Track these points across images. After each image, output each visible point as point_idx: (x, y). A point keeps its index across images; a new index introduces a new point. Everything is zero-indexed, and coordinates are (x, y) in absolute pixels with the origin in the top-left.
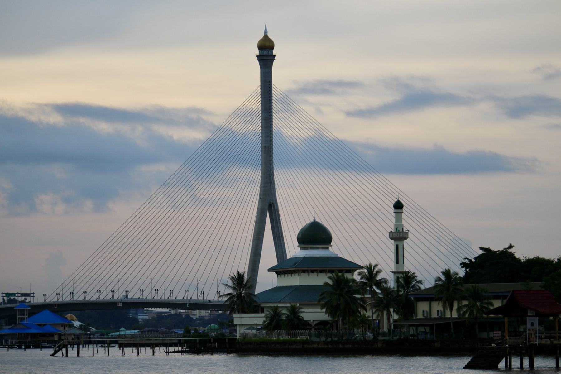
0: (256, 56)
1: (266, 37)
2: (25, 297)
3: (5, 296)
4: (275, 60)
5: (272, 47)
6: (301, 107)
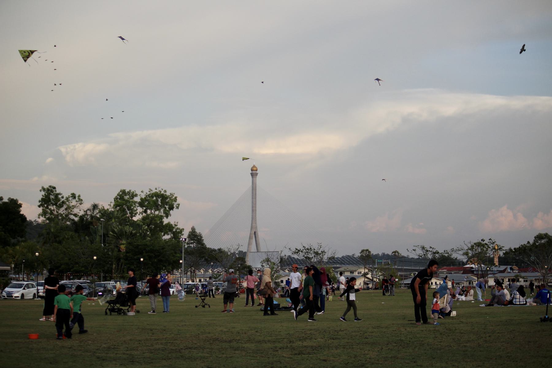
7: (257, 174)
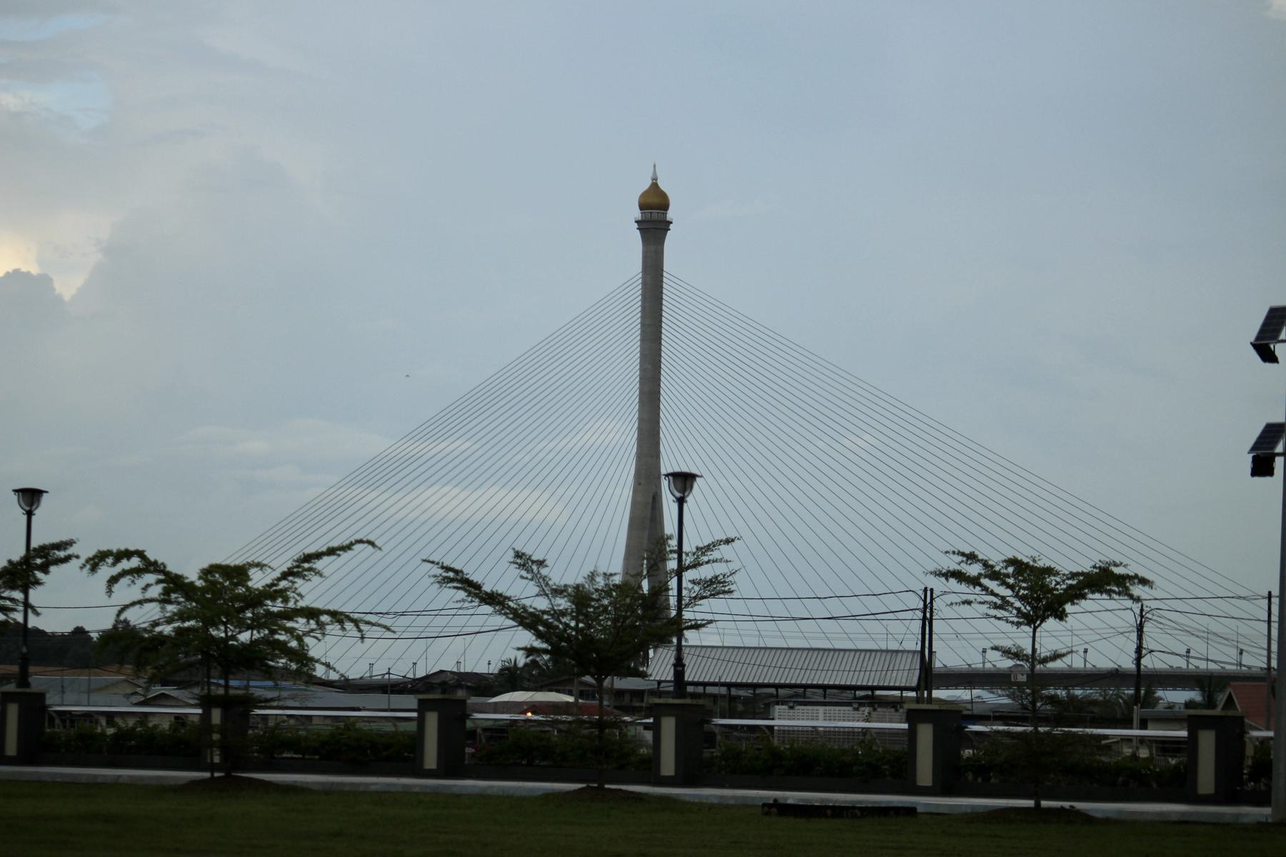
0: (636, 222)
1: (655, 186)
2: (683, 590)
4: (670, 230)
5: (664, 206)
7: (665, 225)
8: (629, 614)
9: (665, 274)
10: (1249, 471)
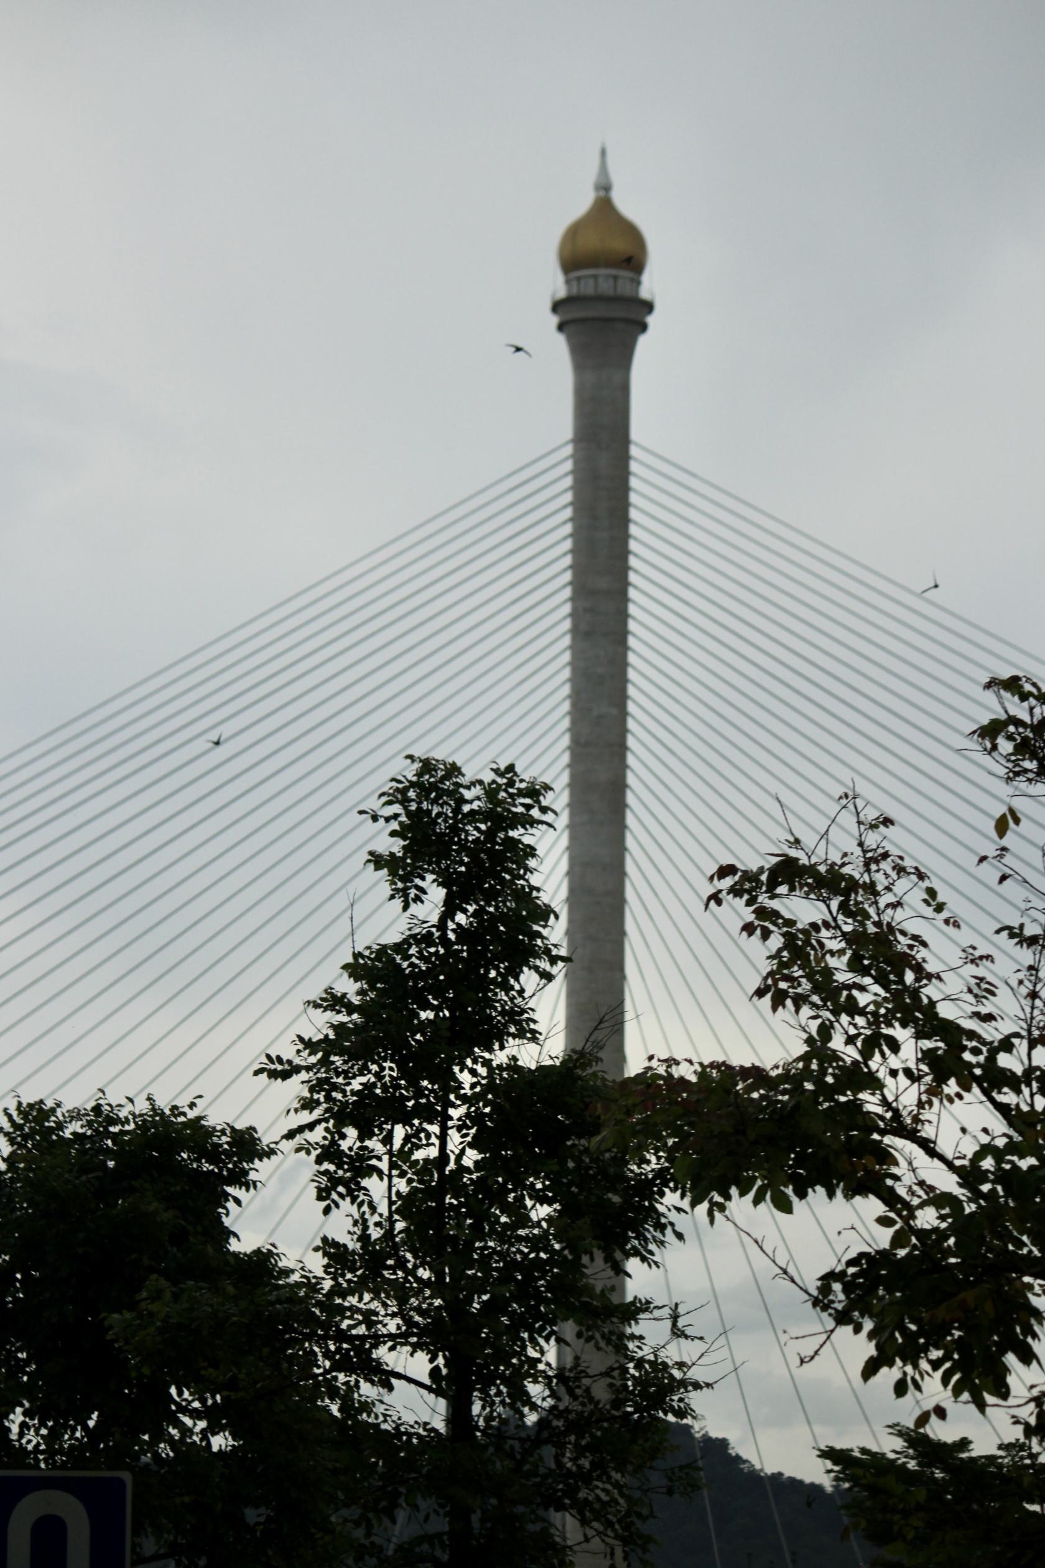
3: (890, 1198)
6: (786, 1371)
8: (527, 1557)
9: (634, 451)
10: (315, 1197)
